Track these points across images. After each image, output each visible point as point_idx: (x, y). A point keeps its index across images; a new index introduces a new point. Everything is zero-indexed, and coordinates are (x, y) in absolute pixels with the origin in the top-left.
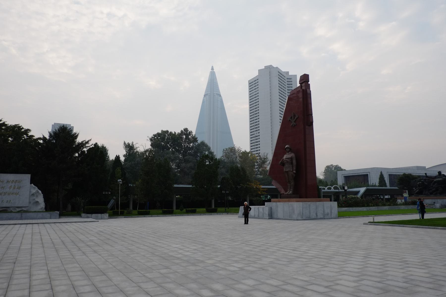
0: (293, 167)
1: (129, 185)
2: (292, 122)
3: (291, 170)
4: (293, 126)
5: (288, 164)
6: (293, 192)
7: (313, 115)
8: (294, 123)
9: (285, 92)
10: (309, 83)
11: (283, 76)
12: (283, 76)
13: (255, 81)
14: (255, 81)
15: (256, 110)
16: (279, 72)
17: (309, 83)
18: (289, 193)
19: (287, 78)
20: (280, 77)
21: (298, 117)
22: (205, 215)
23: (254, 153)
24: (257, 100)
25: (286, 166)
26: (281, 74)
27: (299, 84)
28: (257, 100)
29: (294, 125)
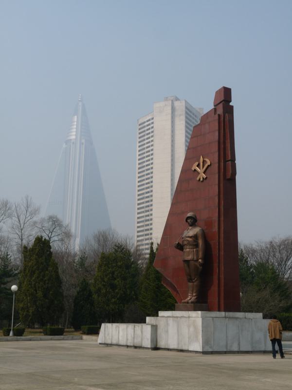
4: (201, 180)
6: (196, 298)
7: (236, 162)
8: (203, 174)
10: (231, 104)
11: (193, 114)
12: (193, 114)
13: (148, 121)
14: (148, 121)
15: (147, 209)
17: (231, 104)
18: (190, 301)
21: (210, 165)
23: (141, 248)
24: (151, 152)
28: (151, 152)
29: (203, 178)
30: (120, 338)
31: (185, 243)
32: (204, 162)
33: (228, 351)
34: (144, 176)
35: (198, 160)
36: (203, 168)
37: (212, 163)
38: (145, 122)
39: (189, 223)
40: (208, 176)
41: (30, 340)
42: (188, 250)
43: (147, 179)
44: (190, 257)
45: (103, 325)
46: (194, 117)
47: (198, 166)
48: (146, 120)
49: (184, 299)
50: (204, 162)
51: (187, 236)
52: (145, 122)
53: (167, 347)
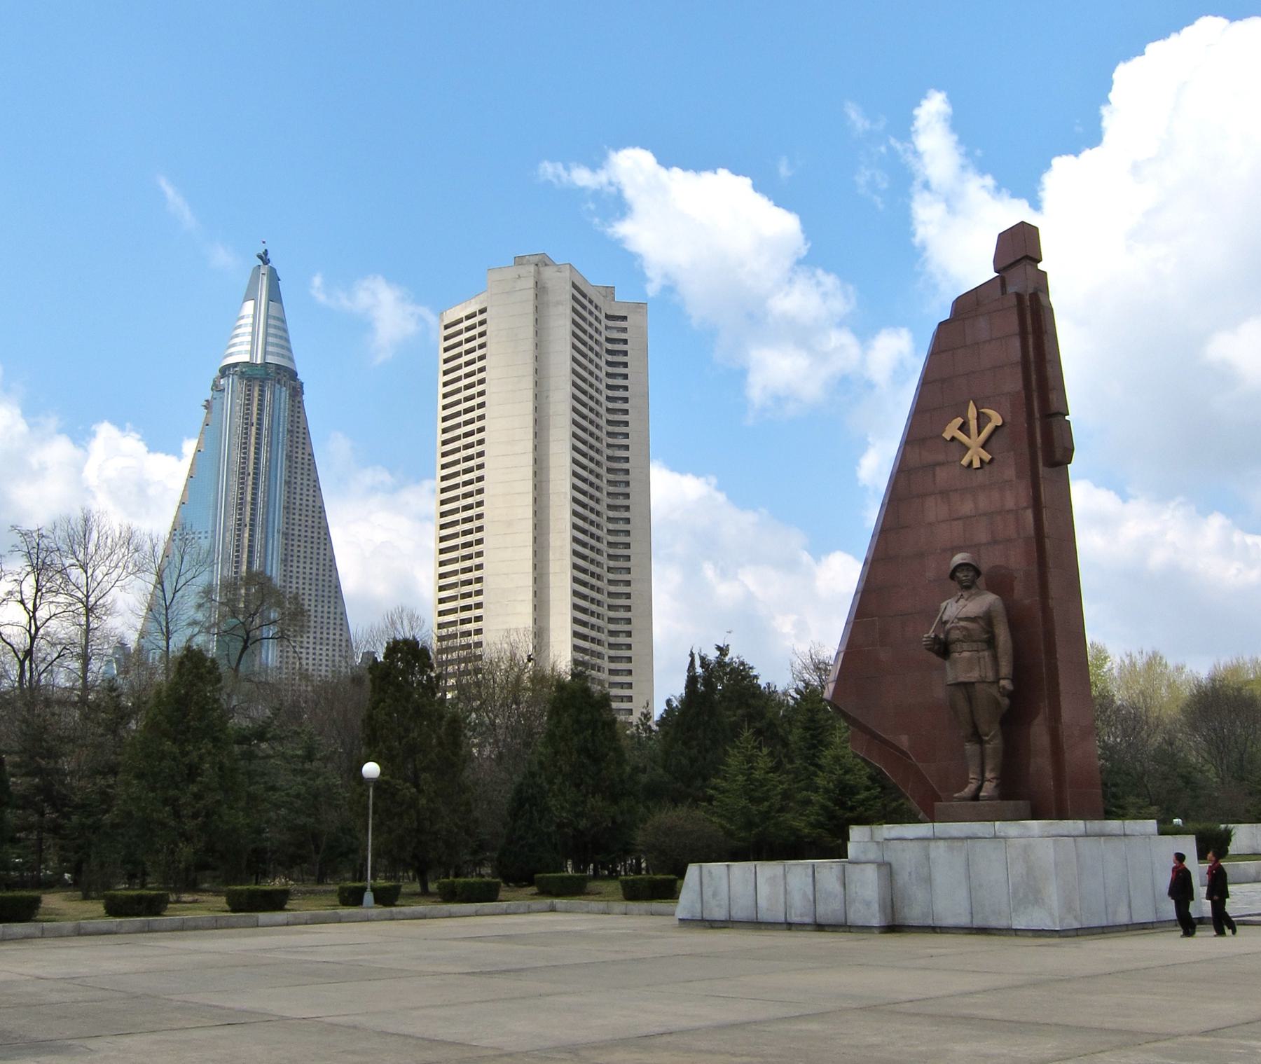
0: (995, 659)
1: (37, 780)
2: (967, 449)
3: (990, 676)
5: (975, 646)
8: (981, 450)
9: (596, 372)
10: (1041, 266)
11: (591, 302)
12: (591, 302)
13: (468, 318)
14: (468, 318)
16: (574, 286)
17: (1041, 266)
19: (608, 313)
20: (579, 308)
22: (850, 932)
25: (963, 654)
26: (584, 296)
27: (996, 272)
29: (982, 461)
30: (762, 902)
31: (955, 635)
32: (982, 420)
33: (975, 926)
34: (456, 462)
35: (964, 415)
36: (979, 433)
37: (1006, 420)
38: (460, 321)
39: (960, 582)
40: (995, 456)
41: (506, 913)
42: (966, 654)
43: (466, 471)
44: (974, 676)
45: (693, 870)
46: (593, 309)
47: (964, 428)
48: (463, 315)
49: (960, 790)
50: (982, 420)
51: (961, 615)
52: (460, 321)
53: (930, 922)
